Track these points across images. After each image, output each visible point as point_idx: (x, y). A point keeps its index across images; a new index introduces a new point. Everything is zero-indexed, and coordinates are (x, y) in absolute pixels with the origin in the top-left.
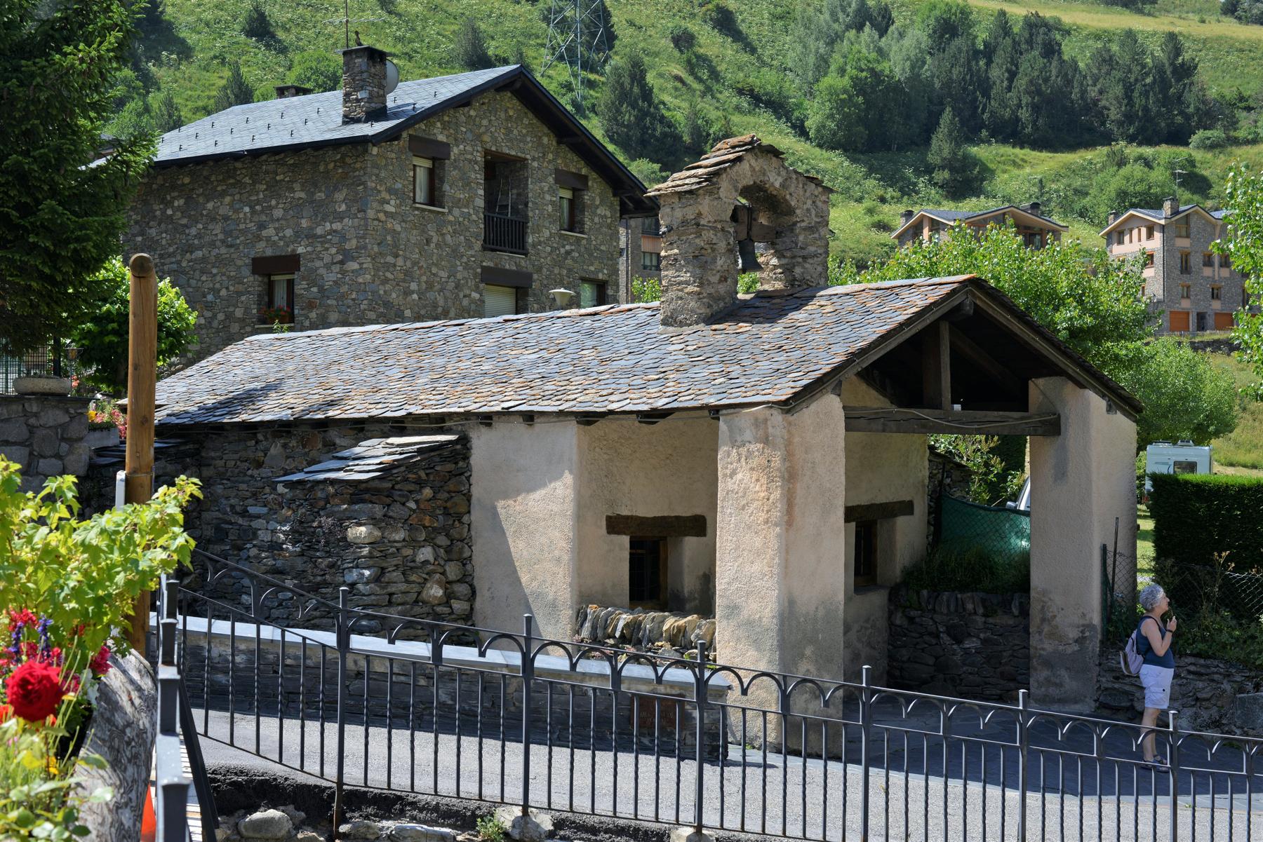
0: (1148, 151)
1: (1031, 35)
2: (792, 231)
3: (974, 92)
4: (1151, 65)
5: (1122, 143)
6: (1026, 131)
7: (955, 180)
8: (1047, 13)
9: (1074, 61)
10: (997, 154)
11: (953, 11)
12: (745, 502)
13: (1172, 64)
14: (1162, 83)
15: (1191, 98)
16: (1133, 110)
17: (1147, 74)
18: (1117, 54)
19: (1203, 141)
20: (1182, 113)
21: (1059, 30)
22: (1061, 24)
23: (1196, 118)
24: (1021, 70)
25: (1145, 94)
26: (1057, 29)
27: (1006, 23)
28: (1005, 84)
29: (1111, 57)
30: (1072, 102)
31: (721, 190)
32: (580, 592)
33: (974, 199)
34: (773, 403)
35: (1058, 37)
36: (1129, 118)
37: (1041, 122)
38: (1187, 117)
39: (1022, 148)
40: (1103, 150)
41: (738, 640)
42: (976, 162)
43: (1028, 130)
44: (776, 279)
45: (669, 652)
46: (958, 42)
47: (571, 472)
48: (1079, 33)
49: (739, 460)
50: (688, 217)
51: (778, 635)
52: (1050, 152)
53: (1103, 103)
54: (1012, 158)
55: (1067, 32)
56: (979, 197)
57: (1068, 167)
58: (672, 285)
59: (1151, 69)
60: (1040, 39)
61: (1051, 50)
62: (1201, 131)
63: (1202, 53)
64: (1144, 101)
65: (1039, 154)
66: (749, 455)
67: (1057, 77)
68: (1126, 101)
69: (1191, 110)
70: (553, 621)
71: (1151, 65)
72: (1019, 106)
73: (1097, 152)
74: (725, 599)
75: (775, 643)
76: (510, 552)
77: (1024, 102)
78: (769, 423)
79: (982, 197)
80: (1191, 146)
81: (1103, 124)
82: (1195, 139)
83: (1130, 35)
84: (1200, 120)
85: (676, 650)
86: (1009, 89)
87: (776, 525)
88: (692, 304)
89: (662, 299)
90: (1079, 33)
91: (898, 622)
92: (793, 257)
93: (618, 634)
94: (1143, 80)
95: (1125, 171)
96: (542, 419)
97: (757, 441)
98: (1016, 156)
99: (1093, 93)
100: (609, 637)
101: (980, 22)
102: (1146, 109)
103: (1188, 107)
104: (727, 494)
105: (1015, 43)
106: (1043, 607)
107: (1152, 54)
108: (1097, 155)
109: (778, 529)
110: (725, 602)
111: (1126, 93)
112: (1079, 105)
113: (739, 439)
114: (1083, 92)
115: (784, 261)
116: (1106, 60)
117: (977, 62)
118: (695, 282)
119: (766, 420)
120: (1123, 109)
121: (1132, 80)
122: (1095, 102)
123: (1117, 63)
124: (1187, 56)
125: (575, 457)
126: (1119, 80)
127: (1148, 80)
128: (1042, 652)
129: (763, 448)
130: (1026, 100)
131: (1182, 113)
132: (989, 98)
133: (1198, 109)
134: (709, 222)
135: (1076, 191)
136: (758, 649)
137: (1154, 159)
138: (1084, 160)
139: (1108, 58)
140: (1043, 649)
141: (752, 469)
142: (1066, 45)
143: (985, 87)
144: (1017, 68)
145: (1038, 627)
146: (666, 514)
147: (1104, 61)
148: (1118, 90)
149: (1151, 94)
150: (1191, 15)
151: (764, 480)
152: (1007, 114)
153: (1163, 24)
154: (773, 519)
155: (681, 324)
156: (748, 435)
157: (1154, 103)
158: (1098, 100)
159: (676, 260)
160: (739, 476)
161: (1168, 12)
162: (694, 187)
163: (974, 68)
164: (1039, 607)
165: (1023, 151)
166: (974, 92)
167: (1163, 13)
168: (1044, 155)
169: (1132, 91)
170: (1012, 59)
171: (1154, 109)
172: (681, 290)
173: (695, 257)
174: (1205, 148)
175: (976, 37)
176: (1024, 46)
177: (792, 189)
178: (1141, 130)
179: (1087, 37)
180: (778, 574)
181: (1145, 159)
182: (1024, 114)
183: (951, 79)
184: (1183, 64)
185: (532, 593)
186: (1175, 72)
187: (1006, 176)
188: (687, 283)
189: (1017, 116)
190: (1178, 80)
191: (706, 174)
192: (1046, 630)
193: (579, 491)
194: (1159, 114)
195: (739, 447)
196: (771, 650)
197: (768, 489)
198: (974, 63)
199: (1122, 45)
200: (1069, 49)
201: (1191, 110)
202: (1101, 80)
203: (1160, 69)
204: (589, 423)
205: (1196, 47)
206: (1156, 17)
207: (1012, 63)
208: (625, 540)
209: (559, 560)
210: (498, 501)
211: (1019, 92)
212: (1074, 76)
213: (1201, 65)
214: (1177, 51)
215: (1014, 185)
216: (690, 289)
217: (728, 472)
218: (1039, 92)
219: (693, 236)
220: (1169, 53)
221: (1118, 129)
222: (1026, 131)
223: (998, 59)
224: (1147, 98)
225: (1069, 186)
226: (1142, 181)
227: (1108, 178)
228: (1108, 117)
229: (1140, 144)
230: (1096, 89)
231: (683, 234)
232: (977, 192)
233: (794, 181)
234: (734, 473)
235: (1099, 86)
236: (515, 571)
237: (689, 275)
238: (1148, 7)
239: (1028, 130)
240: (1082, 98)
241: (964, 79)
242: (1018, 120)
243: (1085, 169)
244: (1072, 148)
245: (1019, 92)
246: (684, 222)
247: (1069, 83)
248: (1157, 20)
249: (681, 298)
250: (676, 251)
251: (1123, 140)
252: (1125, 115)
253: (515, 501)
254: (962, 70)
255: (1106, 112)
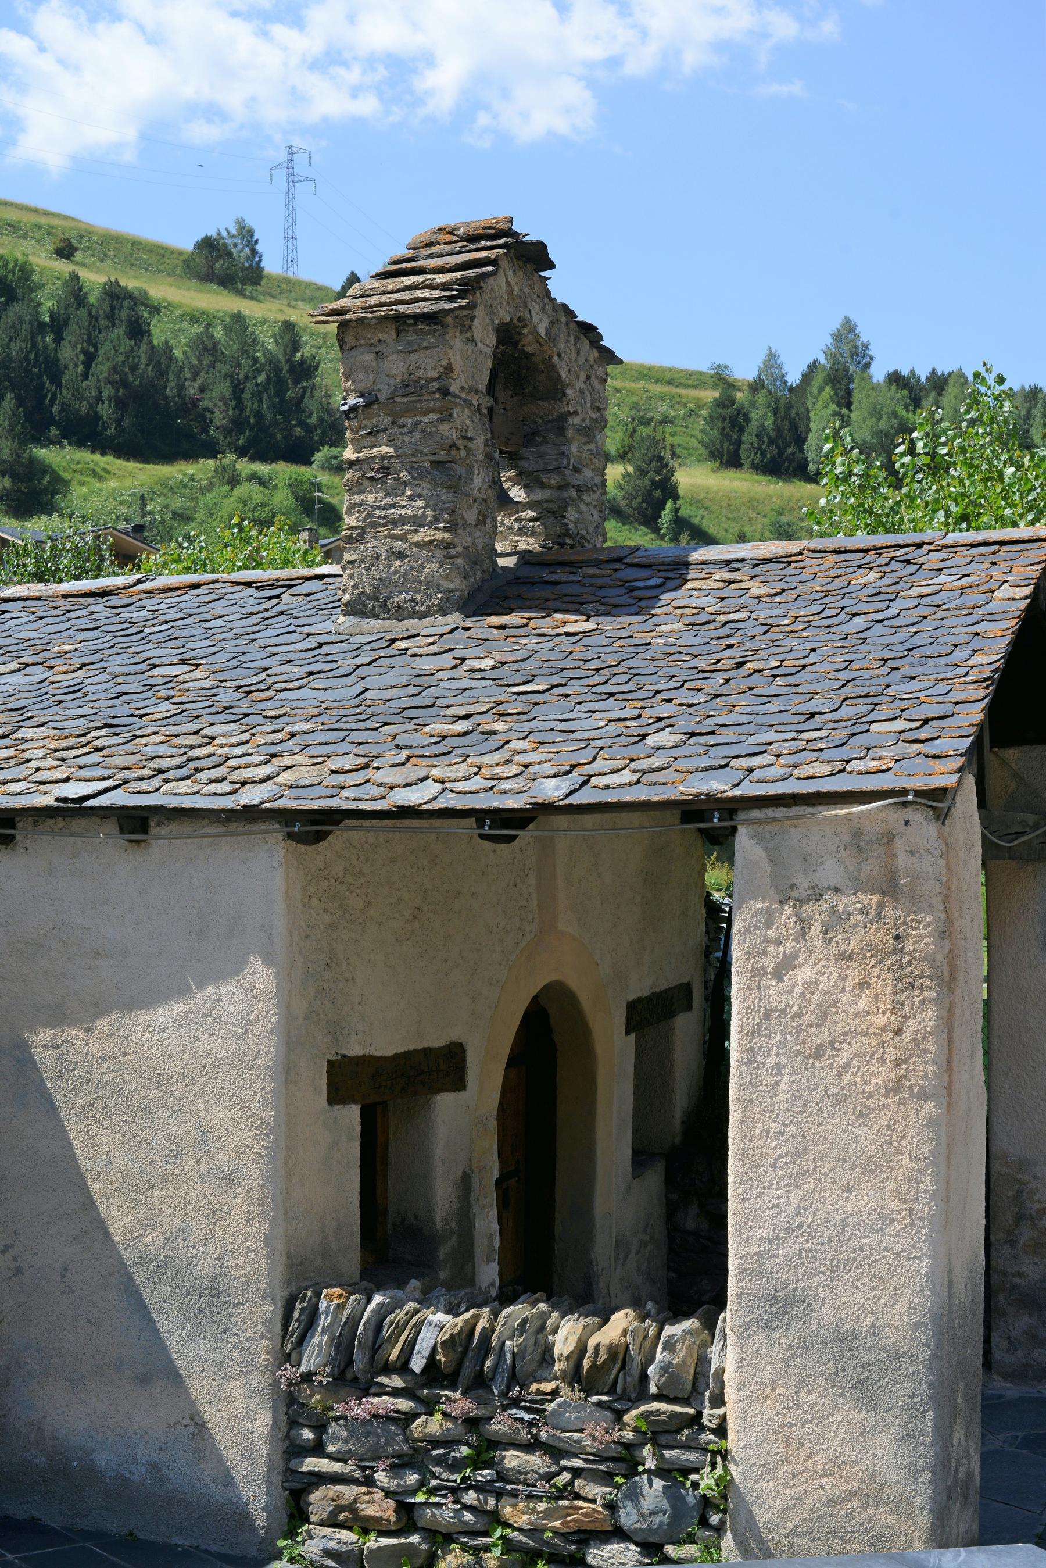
0: (263, 468)
1: (113, 308)
2: (561, 430)
3: (40, 376)
4: (263, 360)
5: (231, 457)
6: (109, 432)
7: (19, 490)
8: (130, 283)
9: (168, 348)
10: (72, 460)
11: (11, 265)
12: (824, 1038)
13: (289, 361)
14: (278, 384)
15: (311, 405)
16: (243, 415)
17: (259, 371)
18: (223, 342)
19: (328, 460)
20: (302, 423)
21: (147, 306)
22: (147, 299)
23: (319, 431)
24: (101, 352)
25: (258, 395)
26: (143, 304)
27: (80, 289)
28: (80, 369)
29: (215, 345)
30: (166, 398)
31: (476, 322)
32: (289, 1256)
33: (44, 518)
34: (918, 793)
35: (146, 315)
36: (238, 425)
37: (126, 422)
38: (309, 429)
39: (103, 454)
40: (211, 464)
41: (805, 1382)
42: (45, 469)
43: (111, 431)
44: (521, 532)
45: (577, 1408)
46: (17, 308)
47: (268, 960)
48: (172, 312)
49: (803, 933)
50: (420, 373)
51: (930, 1371)
52: (140, 462)
53: (205, 403)
54: (91, 466)
55: (156, 310)
56: (50, 515)
57: (163, 482)
58: (374, 525)
59: (263, 365)
60: (124, 314)
61: (138, 331)
62: (327, 448)
63: (323, 351)
64: (256, 404)
65: (125, 463)
66: (835, 922)
67: (147, 365)
68: (234, 403)
69: (313, 420)
70: (211, 1330)
71: (263, 360)
72: (99, 399)
73: (200, 465)
74: (758, 1280)
75: (923, 1389)
76: (74, 1158)
77: (105, 394)
78: (899, 842)
79: (55, 515)
80: (314, 466)
81: (205, 430)
82: (319, 457)
83: (238, 318)
84: (324, 433)
85: (599, 1404)
86: (85, 376)
87: (924, 1095)
88: (432, 569)
89: (347, 557)
90: (172, 312)
91: (690, 1224)
92: (563, 487)
93: (417, 1364)
94: (255, 377)
95: (241, 490)
96: (173, 827)
97: (859, 886)
98: (96, 464)
99: (192, 390)
100: (387, 1369)
101: (44, 285)
102: (259, 415)
103: (310, 416)
104: (767, 1016)
105: (94, 318)
106: (1019, 1193)
107: (263, 346)
108: (201, 469)
109: (929, 1107)
110: (760, 1286)
111: (234, 392)
112: (176, 403)
113: (803, 882)
114: (181, 388)
115: (540, 495)
116: (208, 348)
117: (43, 337)
118: (436, 519)
119: (888, 838)
120: (230, 412)
121: (241, 376)
122: (195, 403)
123: (223, 353)
124: (307, 351)
125: (280, 923)
126: (226, 376)
127: (262, 379)
128: (1017, 1280)
129: (880, 906)
130: (107, 391)
131: (302, 423)
132: (59, 385)
133: (321, 420)
134: (462, 388)
135: (176, 515)
136: (868, 1404)
137: (271, 479)
138: (185, 475)
139: (210, 346)
140: (1020, 1275)
141: (845, 957)
142: (155, 326)
143: (54, 370)
144: (96, 350)
145: (1009, 1232)
146: (411, 1048)
147: (206, 349)
148: (224, 388)
149: (265, 397)
150: (300, 303)
151: (885, 984)
152: (84, 408)
153: (270, 310)
154: (916, 1080)
155: (400, 613)
156: (830, 872)
157: (268, 408)
158: (199, 400)
159: (385, 470)
160: (804, 974)
161: (274, 297)
162: (434, 307)
163: (41, 345)
164: (1011, 1193)
165: (105, 459)
166: (40, 376)
167: (268, 298)
168: (132, 465)
169: (242, 391)
170: (90, 337)
171: (269, 416)
172: (402, 537)
173: (437, 464)
174: (330, 469)
175: (39, 305)
176: (103, 322)
177: (562, 345)
178: (252, 443)
179: (181, 318)
180: (931, 1218)
181: (260, 479)
182: (105, 410)
183: (8, 355)
184: (302, 361)
185: (144, 1260)
186: (292, 369)
187: (84, 489)
188: (418, 522)
189: (96, 413)
190: (296, 382)
191: (457, 282)
192: (1024, 1238)
193: (288, 1005)
194: (275, 423)
195: (801, 902)
196: (907, 1407)
197: (897, 1007)
198: (40, 337)
199: (228, 330)
200: (159, 332)
201: (313, 420)
202: (202, 374)
203: (272, 362)
204: (319, 837)
205: (315, 343)
206: (260, 301)
207: (89, 342)
208: (353, 1113)
209: (230, 1179)
210: (32, 1028)
211: (99, 381)
212: (168, 367)
213: (322, 365)
214: (295, 345)
215: (96, 502)
216: (425, 534)
217: (770, 964)
218: (124, 383)
219: (434, 416)
220: (286, 346)
221: (225, 438)
222: (109, 432)
223: (71, 335)
224: (261, 401)
225: (166, 507)
226: (263, 505)
227: (219, 500)
228: (211, 421)
229: (252, 459)
230: (196, 385)
231: (408, 411)
232: (48, 509)
233: (564, 329)
234: (786, 966)
235: (199, 381)
236: (90, 1205)
237: (421, 503)
238: (248, 289)
239: (111, 431)
240: (179, 395)
241: (26, 358)
242: (97, 417)
243: (185, 486)
244: (168, 458)
245: (99, 381)
246: (410, 386)
247: (162, 373)
248: (262, 305)
249: (401, 555)
250: (385, 449)
251: (231, 452)
252: (233, 421)
253: (88, 1031)
254: (23, 345)
255: (209, 415)
